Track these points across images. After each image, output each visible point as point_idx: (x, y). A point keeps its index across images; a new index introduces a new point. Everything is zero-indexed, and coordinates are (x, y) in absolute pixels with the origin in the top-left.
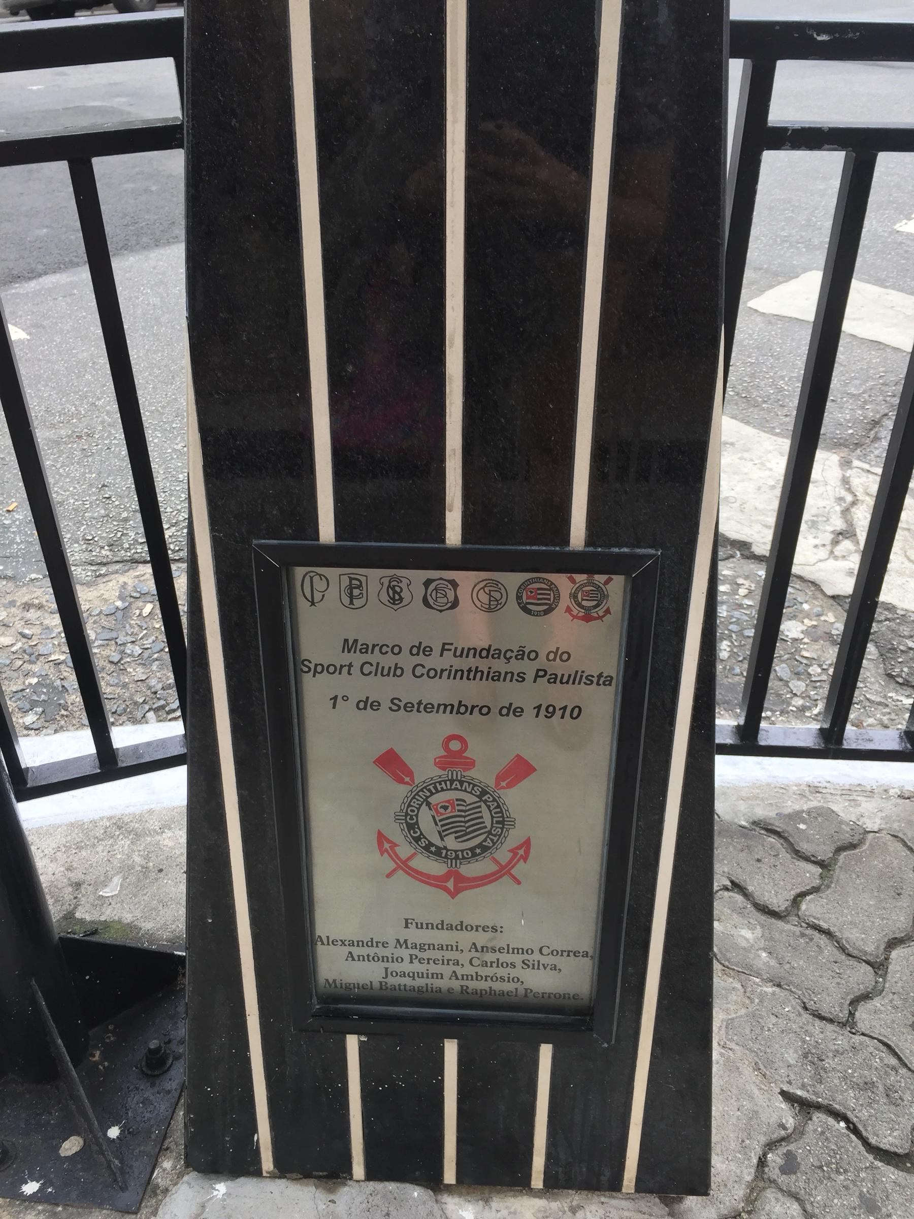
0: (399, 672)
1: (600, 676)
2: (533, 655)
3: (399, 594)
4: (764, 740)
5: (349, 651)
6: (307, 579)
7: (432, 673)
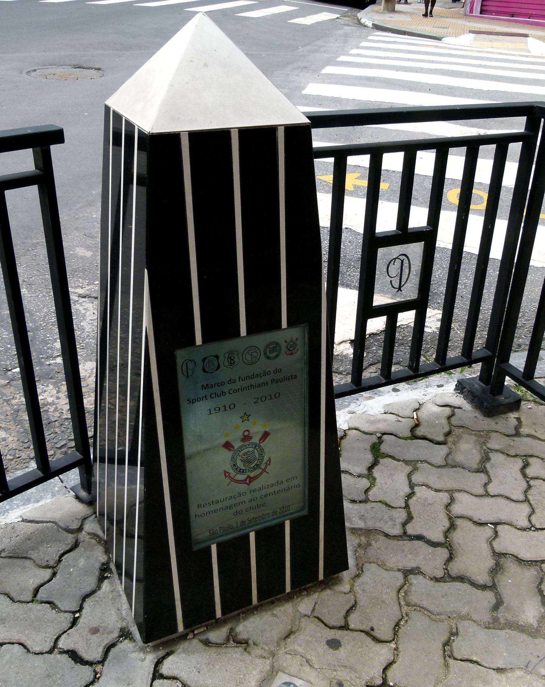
0: (224, 394)
1: (292, 376)
2: (269, 373)
3: (233, 360)
4: (364, 384)
5: (205, 389)
6: (185, 365)
7: (235, 391)
